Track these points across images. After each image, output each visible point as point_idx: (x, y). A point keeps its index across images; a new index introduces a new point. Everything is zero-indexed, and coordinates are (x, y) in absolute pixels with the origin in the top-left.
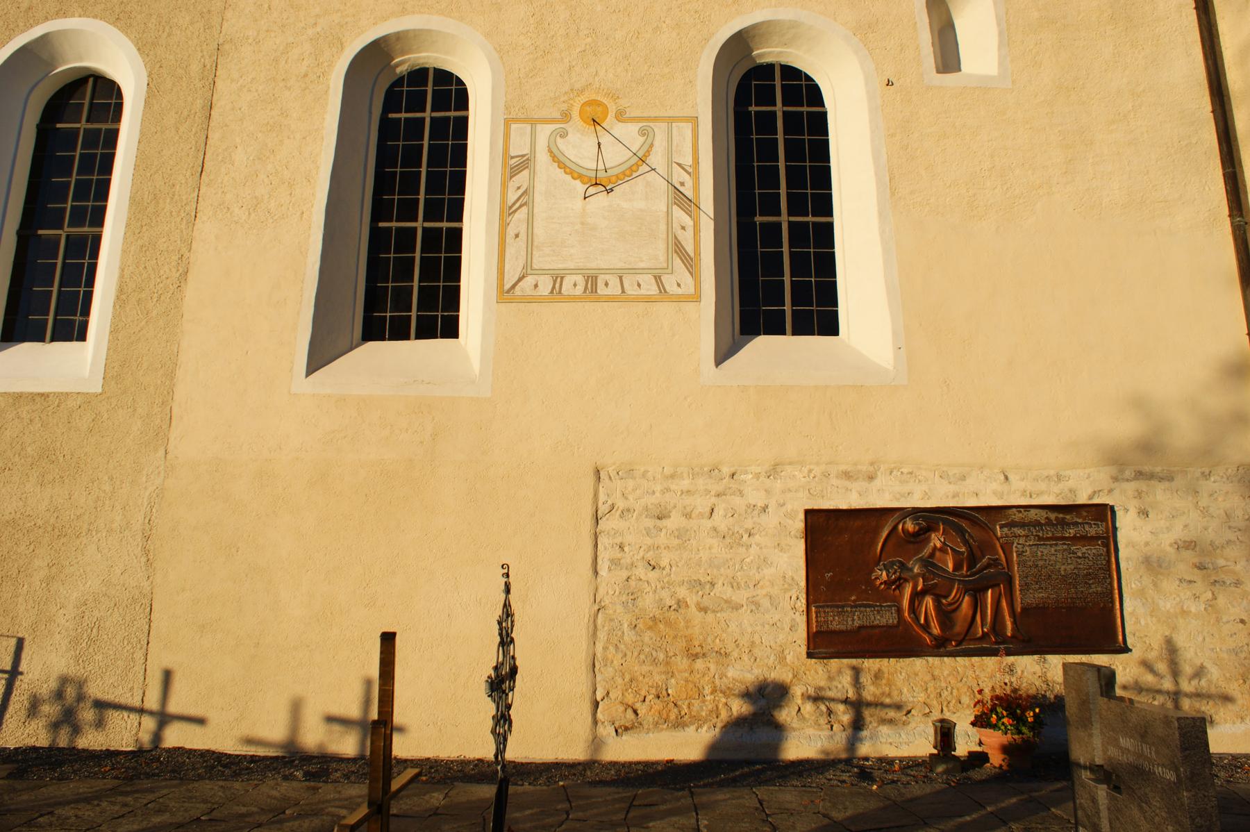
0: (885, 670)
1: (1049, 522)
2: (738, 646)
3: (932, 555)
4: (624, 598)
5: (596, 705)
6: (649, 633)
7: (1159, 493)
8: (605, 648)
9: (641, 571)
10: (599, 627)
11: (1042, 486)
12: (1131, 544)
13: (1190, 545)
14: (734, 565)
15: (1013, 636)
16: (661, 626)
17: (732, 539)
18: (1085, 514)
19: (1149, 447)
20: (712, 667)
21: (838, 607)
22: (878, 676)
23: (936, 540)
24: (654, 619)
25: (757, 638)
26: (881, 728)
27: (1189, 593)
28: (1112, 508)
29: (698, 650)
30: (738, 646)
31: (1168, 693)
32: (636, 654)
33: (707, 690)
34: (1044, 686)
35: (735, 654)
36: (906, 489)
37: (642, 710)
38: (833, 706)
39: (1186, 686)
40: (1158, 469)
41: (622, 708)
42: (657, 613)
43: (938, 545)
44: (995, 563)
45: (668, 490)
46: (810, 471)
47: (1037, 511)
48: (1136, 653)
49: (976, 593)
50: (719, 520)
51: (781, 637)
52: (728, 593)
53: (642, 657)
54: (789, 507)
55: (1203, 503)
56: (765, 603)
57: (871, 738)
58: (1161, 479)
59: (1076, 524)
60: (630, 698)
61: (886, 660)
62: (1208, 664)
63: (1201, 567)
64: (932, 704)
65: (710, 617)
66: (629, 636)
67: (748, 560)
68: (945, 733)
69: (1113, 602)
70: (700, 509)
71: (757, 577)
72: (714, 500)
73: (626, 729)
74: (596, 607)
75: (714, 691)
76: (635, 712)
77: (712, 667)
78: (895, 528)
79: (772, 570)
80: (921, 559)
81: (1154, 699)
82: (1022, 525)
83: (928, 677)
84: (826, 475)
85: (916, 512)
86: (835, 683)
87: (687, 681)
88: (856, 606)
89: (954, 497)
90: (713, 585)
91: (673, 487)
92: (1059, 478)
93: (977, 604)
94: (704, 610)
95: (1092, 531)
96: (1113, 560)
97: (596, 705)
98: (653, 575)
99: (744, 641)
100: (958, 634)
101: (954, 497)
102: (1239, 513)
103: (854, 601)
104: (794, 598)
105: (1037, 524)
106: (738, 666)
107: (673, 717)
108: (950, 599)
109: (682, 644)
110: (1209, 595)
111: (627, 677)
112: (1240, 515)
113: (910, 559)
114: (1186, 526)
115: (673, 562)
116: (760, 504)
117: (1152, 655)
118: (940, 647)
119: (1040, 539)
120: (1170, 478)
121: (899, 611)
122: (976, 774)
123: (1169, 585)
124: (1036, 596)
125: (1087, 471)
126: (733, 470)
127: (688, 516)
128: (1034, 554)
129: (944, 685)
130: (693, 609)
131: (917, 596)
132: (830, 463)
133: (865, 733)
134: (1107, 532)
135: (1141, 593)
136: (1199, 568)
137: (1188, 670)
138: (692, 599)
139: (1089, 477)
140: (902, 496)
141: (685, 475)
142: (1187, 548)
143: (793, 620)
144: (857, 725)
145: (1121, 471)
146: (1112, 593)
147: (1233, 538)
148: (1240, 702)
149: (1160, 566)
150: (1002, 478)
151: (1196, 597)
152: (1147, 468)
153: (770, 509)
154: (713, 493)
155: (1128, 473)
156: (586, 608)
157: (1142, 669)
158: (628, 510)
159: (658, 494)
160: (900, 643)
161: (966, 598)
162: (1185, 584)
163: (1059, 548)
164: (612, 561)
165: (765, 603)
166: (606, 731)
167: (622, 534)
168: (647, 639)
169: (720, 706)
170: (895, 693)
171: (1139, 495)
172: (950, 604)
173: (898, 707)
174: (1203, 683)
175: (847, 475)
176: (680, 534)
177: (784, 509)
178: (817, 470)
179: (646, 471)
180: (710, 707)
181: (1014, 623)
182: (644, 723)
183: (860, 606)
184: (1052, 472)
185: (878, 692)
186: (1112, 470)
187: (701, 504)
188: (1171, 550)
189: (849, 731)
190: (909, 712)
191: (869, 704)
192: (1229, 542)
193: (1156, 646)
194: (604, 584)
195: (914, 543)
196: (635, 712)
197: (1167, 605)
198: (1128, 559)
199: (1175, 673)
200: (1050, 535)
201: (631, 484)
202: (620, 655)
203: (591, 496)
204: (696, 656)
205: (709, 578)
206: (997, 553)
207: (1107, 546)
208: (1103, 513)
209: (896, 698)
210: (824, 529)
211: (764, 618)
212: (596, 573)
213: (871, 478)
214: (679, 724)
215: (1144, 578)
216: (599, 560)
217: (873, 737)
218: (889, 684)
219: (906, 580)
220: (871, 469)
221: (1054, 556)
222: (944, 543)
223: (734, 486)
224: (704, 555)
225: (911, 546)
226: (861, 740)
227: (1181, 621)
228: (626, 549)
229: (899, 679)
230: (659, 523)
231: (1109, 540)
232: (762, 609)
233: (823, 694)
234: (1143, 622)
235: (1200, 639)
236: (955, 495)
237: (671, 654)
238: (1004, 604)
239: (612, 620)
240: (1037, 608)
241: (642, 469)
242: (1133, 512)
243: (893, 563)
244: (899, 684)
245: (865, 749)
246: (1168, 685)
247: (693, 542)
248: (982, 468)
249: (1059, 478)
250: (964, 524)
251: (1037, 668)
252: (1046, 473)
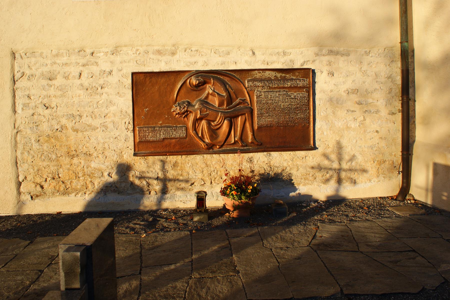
0: (179, 161)
2: (96, 150)
3: (207, 97)
4: (31, 125)
5: (19, 184)
6: (46, 144)
7: (341, 62)
8: (22, 153)
9: (41, 110)
10: (18, 142)
11: (274, 58)
12: (323, 91)
13: (355, 91)
14: (93, 105)
15: (252, 143)
16: (53, 140)
17: (92, 90)
18: (297, 74)
19: (338, 36)
20: (83, 162)
22: (175, 165)
23: (209, 89)
24: (48, 136)
25: (106, 146)
26: (176, 192)
27: (351, 118)
28: (313, 71)
29: (74, 152)
30: (96, 150)
31: (335, 170)
32: (39, 156)
33: (80, 175)
34: (269, 169)
35: (95, 154)
36: (193, 60)
37: (46, 186)
38: (150, 181)
39: (345, 166)
40: (342, 49)
41: (34, 185)
42: (50, 133)
43: (211, 92)
45: (55, 63)
46: (137, 50)
47: (270, 72)
48: (320, 150)
49: (232, 120)
50: (85, 81)
51: (120, 144)
52: (90, 121)
53: (43, 157)
54: (124, 71)
55: (365, 68)
56: (110, 126)
57: (171, 198)
58: (342, 55)
59: (292, 79)
60: (38, 180)
62: (357, 154)
63: (359, 103)
64: (204, 180)
65: (80, 134)
66: (36, 146)
67: (100, 102)
68: (201, 199)
69: (309, 123)
70: (73, 74)
71: (106, 111)
72: (81, 68)
73: (37, 196)
74: (16, 131)
75: (84, 175)
76: (42, 187)
77: (83, 162)
78: (185, 82)
79: (115, 107)
80: (200, 100)
81: (327, 173)
82: (261, 80)
83: (203, 166)
84: (147, 52)
85: (198, 73)
86: (151, 169)
87: (69, 170)
88: (161, 127)
89: (222, 64)
90: (81, 116)
91: (58, 61)
92: (285, 53)
93: (231, 126)
94: (77, 131)
95: (301, 84)
96: (311, 99)
97: (19, 184)
98: (47, 112)
99: (100, 147)
100: (220, 142)
101: (222, 64)
102: (383, 74)
103: (161, 124)
104: (127, 123)
106: (96, 161)
107: (62, 189)
109: (65, 149)
110: (362, 118)
111: (36, 169)
112: (383, 75)
113: (194, 100)
114: (353, 81)
115: (58, 105)
116: (108, 70)
117: (328, 151)
118: (210, 149)
120: (348, 55)
121: (187, 129)
122: (216, 222)
123: (341, 113)
124: (266, 120)
125: (301, 50)
126: (92, 51)
127: (67, 78)
128: (266, 97)
129: (212, 169)
130: (70, 130)
131: (197, 121)
132: (149, 45)
133: (168, 195)
134: (309, 84)
135: (326, 118)
136: (358, 104)
137: (346, 157)
138: (70, 125)
139: (302, 53)
140: (191, 64)
141: (65, 54)
142: (353, 93)
143: (127, 135)
144: (164, 191)
145: (321, 50)
146: (309, 118)
147: (378, 87)
148: (370, 173)
149: (338, 103)
150: (251, 53)
151: (355, 119)
152: (335, 49)
153: (113, 73)
154: (80, 64)
155: (325, 51)
156: (9, 130)
157: (323, 158)
158: (32, 75)
159: (49, 66)
160: (187, 148)
161: (226, 121)
162: (350, 112)
163: (281, 93)
164: (24, 105)
165: (110, 126)
166: (26, 197)
167: (29, 89)
168: (45, 148)
169: (88, 182)
170: (185, 174)
171: (330, 63)
172: (216, 125)
173: (187, 181)
174: (354, 163)
175: (159, 52)
176: (60, 88)
177: (122, 72)
178: (141, 50)
179: (42, 53)
180: (82, 183)
181: (253, 135)
182: (47, 192)
183: (164, 127)
184: (281, 50)
186: (316, 49)
187: (75, 71)
188: (345, 94)
189: (159, 194)
190: (192, 184)
191: (170, 180)
192: (375, 90)
194: (19, 118)
195: (196, 91)
196: (42, 187)
197: (339, 124)
198: (320, 99)
199: (340, 159)
200: (276, 86)
201: (33, 60)
202: (31, 157)
203: (10, 67)
204: (73, 157)
205: (78, 113)
206: (245, 96)
207: (309, 92)
208: (308, 74)
209: (185, 177)
210: (144, 85)
211: (109, 137)
212: (15, 111)
213: (173, 54)
214: (66, 192)
215: (328, 109)
216: (17, 104)
217: (173, 197)
218: (182, 170)
219: (191, 112)
220: (173, 48)
221: (280, 99)
222: (214, 91)
223: (93, 59)
224: (76, 100)
225: (195, 92)
226: (164, 199)
227: (346, 132)
228: (32, 98)
229: (187, 167)
230: (50, 82)
231: (310, 89)
232: (109, 130)
234: (325, 133)
235: (355, 141)
236: (223, 63)
237: (59, 155)
238: (248, 125)
239: (25, 138)
240: (267, 126)
241: (40, 52)
242: (325, 73)
243: (184, 103)
244: (187, 169)
245: (167, 204)
246: (335, 165)
247: (70, 92)
248: (239, 48)
249: (285, 53)
250: (226, 79)
251: (266, 159)
252: (277, 51)
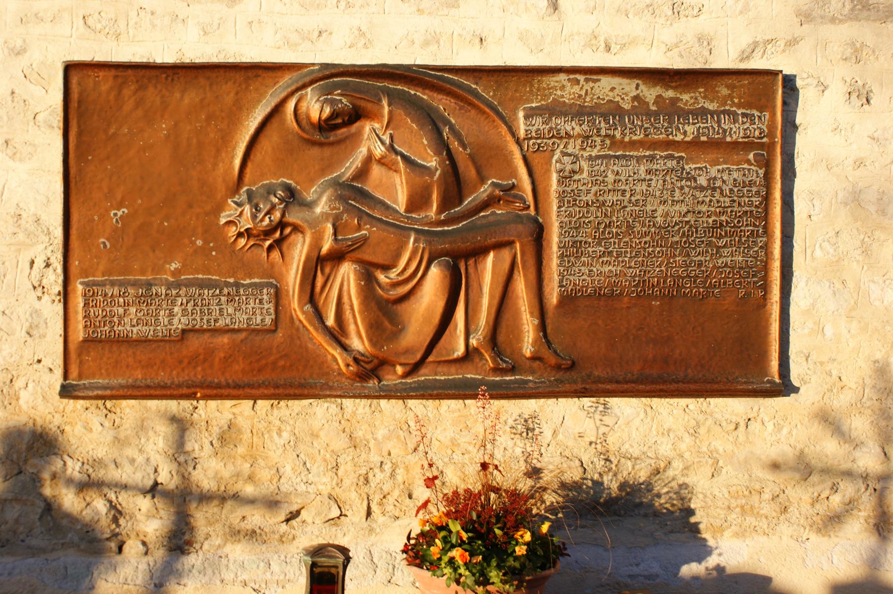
0: (243, 423)
1: (640, 106)
3: (363, 173)
11: (636, 26)
15: (534, 358)
18: (725, 91)
21: (135, 284)
22: (227, 437)
23: (371, 139)
26: (228, 548)
28: (789, 83)
31: (865, 477)
34: (600, 464)
38: (125, 500)
43: (379, 150)
44: (509, 192)
47: (615, 81)
49: (459, 264)
59: (703, 113)
61: (246, 405)
69: (765, 288)
78: (278, 109)
80: (336, 183)
81: (834, 489)
82: (579, 112)
83: (340, 443)
85: (330, 76)
86: (130, 452)
88: (178, 285)
89: (426, 43)
95: (736, 131)
96: (777, 195)
100: (407, 351)
101: (426, 43)
103: (176, 273)
104: (40, 263)
105: (612, 112)
108: (393, 274)
113: (312, 182)
117: (841, 401)
119: (615, 144)
121: (278, 296)
124: (597, 271)
128: (598, 179)
129: (375, 459)
131: (320, 264)
133: (192, 560)
134: (771, 134)
143: (36, 312)
157: (816, 428)
160: (276, 371)
161: (435, 272)
163: (659, 165)
170: (265, 474)
171: (856, 53)
172: (396, 285)
177: (23, 61)
183: (189, 284)
185: (226, 473)
189: (159, 554)
190: (293, 516)
191: (205, 498)
193: (851, 381)
195: (321, 144)
198: (812, 195)
200: (639, 136)
206: (514, 174)
208: (768, 92)
209: (265, 486)
210: (110, 110)
221: (653, 190)
225: (315, 151)
229: (275, 448)
231: (775, 154)
233: (100, 474)
236: (432, 40)
243: (270, 191)
244: (275, 455)
250: (442, 104)
